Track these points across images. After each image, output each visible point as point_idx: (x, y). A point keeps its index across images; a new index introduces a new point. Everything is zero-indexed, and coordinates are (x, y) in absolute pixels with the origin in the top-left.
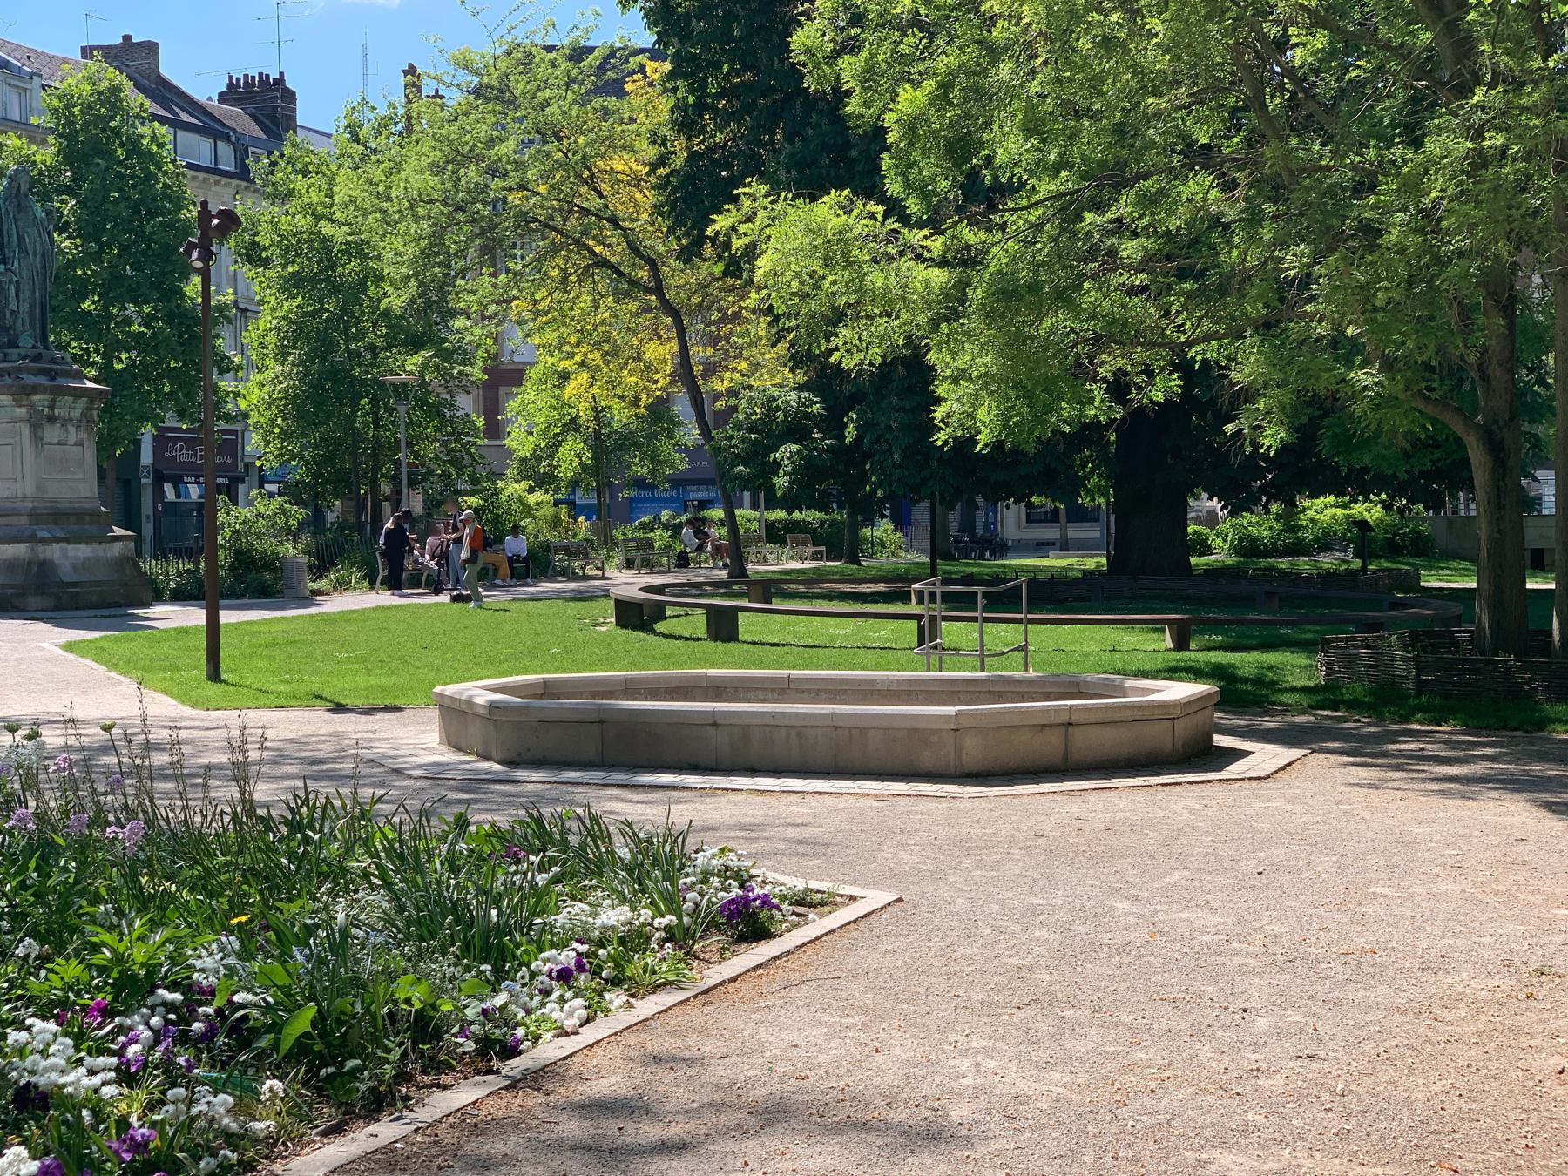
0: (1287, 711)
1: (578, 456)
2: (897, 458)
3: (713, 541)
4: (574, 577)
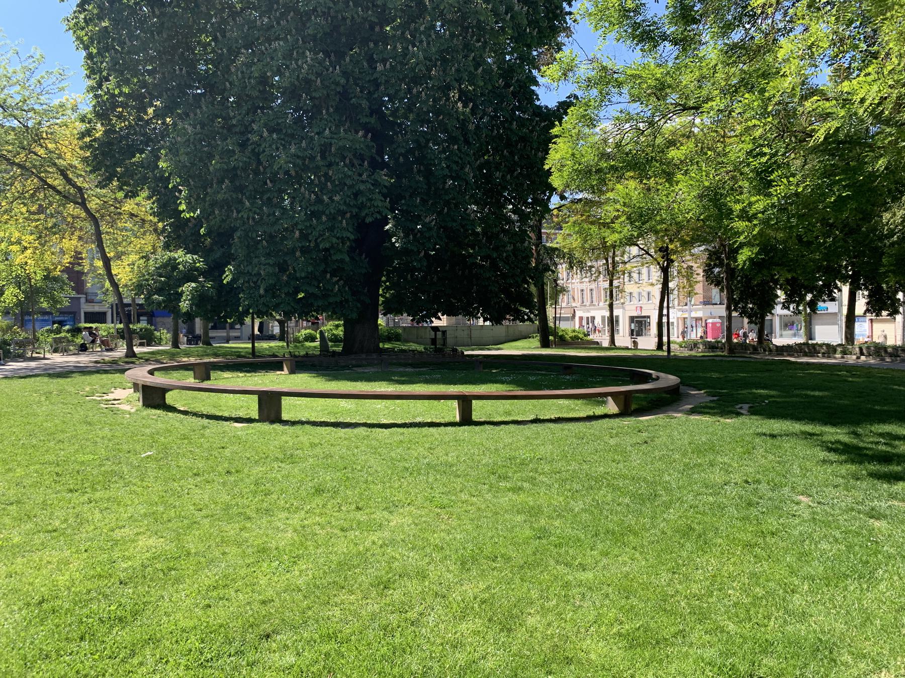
0: (46, 370)
1: (15, 296)
2: (262, 291)
3: (100, 338)
4: (33, 359)
